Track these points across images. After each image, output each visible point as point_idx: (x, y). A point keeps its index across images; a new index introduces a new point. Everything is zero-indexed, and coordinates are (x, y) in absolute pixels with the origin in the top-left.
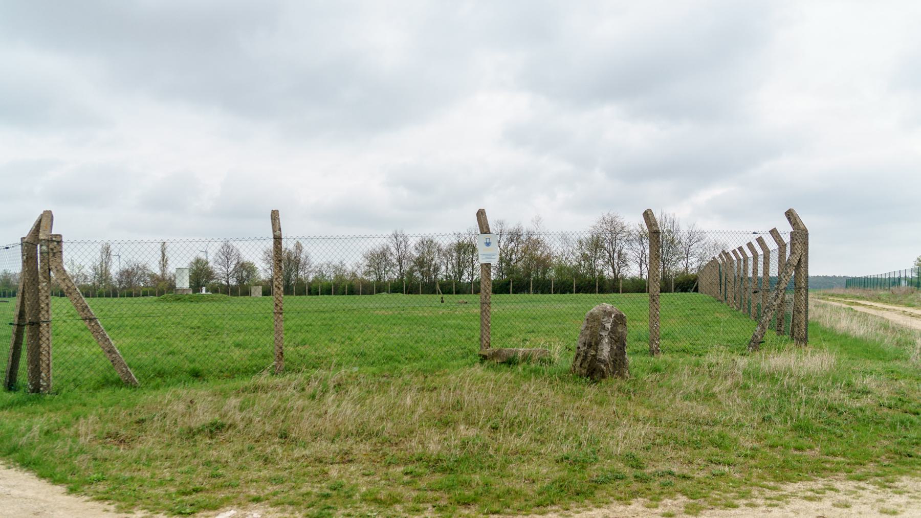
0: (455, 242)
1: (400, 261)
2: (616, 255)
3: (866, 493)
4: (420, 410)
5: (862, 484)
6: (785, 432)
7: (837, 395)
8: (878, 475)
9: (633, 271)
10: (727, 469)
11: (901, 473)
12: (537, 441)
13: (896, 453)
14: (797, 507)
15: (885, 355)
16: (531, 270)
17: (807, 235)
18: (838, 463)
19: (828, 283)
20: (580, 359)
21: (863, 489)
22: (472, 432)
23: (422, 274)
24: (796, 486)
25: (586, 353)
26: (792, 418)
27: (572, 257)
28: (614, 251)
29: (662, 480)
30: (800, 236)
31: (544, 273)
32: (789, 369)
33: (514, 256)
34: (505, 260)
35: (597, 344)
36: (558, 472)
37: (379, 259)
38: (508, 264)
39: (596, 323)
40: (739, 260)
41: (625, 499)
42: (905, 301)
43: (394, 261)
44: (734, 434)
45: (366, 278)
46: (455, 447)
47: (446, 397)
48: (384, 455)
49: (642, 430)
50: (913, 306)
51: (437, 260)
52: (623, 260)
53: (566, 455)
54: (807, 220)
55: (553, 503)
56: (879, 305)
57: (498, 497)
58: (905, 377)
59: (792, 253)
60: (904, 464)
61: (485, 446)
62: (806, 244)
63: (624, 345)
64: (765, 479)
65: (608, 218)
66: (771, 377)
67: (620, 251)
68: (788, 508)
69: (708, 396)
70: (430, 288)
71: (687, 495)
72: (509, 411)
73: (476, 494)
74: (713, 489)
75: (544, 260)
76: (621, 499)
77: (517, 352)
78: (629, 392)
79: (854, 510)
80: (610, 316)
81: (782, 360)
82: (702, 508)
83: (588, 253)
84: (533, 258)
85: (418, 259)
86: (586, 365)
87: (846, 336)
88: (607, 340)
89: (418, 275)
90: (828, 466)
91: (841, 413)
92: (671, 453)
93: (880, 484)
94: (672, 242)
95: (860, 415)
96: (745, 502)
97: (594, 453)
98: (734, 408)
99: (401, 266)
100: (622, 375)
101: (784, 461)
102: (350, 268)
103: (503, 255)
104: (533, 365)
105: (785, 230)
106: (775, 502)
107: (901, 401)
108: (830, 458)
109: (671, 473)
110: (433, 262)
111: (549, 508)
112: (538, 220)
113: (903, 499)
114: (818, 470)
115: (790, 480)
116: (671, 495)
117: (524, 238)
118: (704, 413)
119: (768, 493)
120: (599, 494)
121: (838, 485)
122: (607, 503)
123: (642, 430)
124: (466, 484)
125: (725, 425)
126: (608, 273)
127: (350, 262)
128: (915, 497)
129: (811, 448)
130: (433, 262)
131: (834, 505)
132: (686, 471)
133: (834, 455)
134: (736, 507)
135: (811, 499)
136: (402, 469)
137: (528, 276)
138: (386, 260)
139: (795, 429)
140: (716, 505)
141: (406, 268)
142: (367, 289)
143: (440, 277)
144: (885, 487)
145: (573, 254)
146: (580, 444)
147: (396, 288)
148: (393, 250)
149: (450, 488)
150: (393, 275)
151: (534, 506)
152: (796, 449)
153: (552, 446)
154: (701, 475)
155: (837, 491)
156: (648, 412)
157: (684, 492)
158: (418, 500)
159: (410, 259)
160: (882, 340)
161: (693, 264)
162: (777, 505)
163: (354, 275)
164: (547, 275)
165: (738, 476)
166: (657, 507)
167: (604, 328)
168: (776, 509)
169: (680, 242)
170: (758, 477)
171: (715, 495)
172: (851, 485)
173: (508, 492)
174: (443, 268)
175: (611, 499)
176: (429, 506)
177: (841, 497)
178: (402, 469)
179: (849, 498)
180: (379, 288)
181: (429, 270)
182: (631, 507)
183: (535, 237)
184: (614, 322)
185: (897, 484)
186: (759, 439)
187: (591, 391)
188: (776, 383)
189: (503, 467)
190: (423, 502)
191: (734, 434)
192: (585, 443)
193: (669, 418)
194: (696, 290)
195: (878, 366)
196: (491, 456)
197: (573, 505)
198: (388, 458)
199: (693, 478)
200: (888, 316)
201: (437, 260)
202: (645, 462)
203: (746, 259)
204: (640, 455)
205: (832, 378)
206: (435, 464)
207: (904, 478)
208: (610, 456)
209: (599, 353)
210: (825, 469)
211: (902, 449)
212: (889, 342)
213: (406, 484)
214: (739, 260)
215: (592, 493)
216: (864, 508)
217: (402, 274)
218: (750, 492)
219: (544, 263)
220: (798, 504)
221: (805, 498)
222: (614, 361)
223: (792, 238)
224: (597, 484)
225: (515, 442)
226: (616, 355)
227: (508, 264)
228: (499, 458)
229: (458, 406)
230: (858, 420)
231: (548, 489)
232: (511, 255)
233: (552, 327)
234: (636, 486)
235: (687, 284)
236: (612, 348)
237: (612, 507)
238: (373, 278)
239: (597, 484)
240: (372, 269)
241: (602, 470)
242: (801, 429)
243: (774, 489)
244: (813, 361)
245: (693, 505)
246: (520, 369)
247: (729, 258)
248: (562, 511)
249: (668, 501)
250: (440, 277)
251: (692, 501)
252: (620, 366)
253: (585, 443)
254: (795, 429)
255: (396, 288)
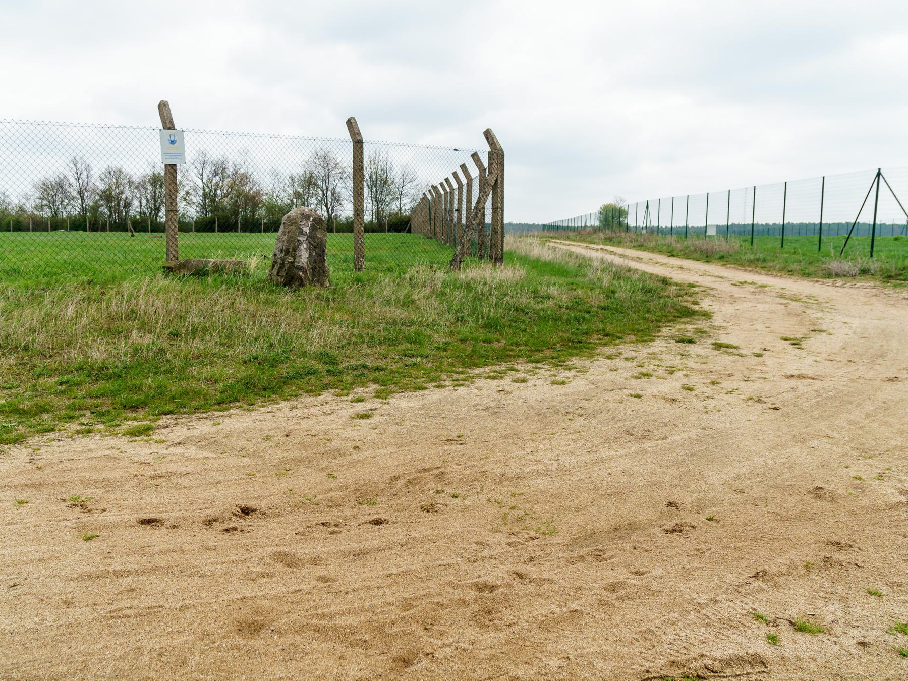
0: (151, 173)
1: (81, 193)
2: (329, 193)
3: (542, 372)
4: (85, 321)
5: (539, 365)
6: (477, 329)
7: (524, 300)
8: (553, 358)
9: (346, 211)
10: (419, 359)
11: (572, 355)
12: (223, 345)
13: (569, 341)
14: (481, 385)
15: (568, 273)
16: (238, 207)
17: (503, 156)
18: (520, 351)
19: (525, 229)
20: (276, 267)
21: (540, 368)
22: (147, 340)
23: (110, 211)
24: (482, 370)
25: (283, 260)
26: (483, 318)
27: (283, 194)
28: (327, 189)
29: (355, 373)
30: (497, 155)
31: (253, 212)
32: (485, 279)
33: (219, 192)
34: (209, 197)
35: (295, 250)
36: (243, 372)
37: (53, 190)
38: (213, 201)
39: (294, 228)
40: (446, 192)
41: (315, 391)
42: (589, 239)
43: (75, 194)
44: (429, 332)
45: (36, 213)
46: (126, 354)
47: (118, 306)
48: (34, 367)
49: (337, 331)
50: (594, 243)
51: (127, 194)
52: (337, 199)
53: (254, 354)
54: (503, 142)
55: (236, 400)
56: (567, 242)
57: (173, 398)
58: (582, 288)
59: (490, 173)
60: (576, 348)
61: (162, 351)
62: (502, 165)
63: (324, 251)
64: (454, 366)
65: (321, 153)
66: (468, 286)
67: (334, 189)
68: (472, 387)
69: (408, 303)
70: (120, 226)
71: (378, 383)
72: (194, 318)
73: (147, 397)
74: (404, 377)
75: (254, 197)
76: (311, 391)
77: (207, 263)
78: (327, 299)
79: (530, 384)
80: (309, 219)
81: (480, 272)
82: (392, 393)
83: (301, 190)
84: (240, 194)
85: (104, 192)
86: (283, 273)
87: (538, 261)
88: (305, 246)
89: (104, 210)
90: (512, 353)
91: (527, 313)
92: (365, 349)
93: (553, 364)
94: (386, 182)
95: (542, 313)
96: (433, 384)
97: (285, 352)
98: (431, 310)
99: (83, 199)
100: (322, 285)
101: (473, 351)
102: (16, 201)
103: (207, 190)
104: (225, 277)
105: (484, 150)
106: (461, 382)
107: (576, 304)
108: (514, 347)
109: (364, 366)
110: (124, 196)
111: (232, 405)
112: (245, 152)
113: (571, 374)
114: (503, 356)
115: (476, 366)
116: (363, 385)
117: (230, 171)
118: (402, 316)
119: (456, 376)
120: (288, 390)
121: (519, 367)
122: (296, 396)
123: (337, 331)
124: (138, 389)
125: (421, 325)
126: (323, 213)
127: (15, 194)
128: (581, 371)
129: (498, 341)
130: (124, 196)
131: (514, 381)
132: (380, 363)
133: (517, 344)
134: (426, 388)
135: (494, 378)
136: (56, 379)
137: (234, 212)
138: (64, 192)
139: (485, 326)
140: (406, 389)
141: (89, 202)
142: (39, 226)
143: (132, 213)
144: (557, 366)
145: (284, 191)
146: (271, 345)
147: (77, 225)
148: (72, 180)
149: (113, 394)
150: (74, 209)
151: (215, 404)
152: (484, 341)
153: (239, 349)
154: (394, 367)
155: (517, 371)
156: (345, 317)
157: (375, 381)
158: (74, 408)
159: (94, 191)
160: (567, 263)
161: (406, 205)
162: (463, 385)
163: (21, 209)
164: (256, 214)
165: (429, 365)
166: (347, 395)
167: (302, 232)
168: (462, 388)
169: (393, 182)
170: (448, 365)
171: (405, 381)
172: (529, 366)
173: (186, 393)
174: (136, 203)
175: (301, 392)
176: (88, 413)
177: (520, 375)
178: (56, 379)
179: (527, 376)
180: (56, 225)
181: (118, 205)
182: (321, 398)
183: (242, 171)
184: (313, 226)
185: (567, 363)
186: (451, 334)
187: (286, 298)
188: (471, 291)
189: (183, 369)
190: (80, 409)
191: (429, 332)
192: (277, 343)
193: (367, 321)
194: (409, 231)
195: (562, 280)
196: (168, 361)
197: (259, 401)
198: (37, 371)
199: (386, 369)
200: (573, 249)
201: (127, 194)
202: (340, 359)
203: (452, 190)
204: (335, 353)
205: (520, 285)
206: (100, 372)
207: (573, 359)
208: (304, 355)
209: (297, 259)
210: (509, 356)
211: (574, 337)
212: (572, 264)
213: (57, 394)
214: (446, 192)
215: (281, 387)
216: (538, 382)
217: (84, 209)
218: (439, 376)
219: (252, 200)
220: (481, 383)
221: (489, 377)
222: (314, 269)
223: (490, 158)
224: (286, 380)
225: (196, 345)
226: (315, 262)
227: (213, 201)
228: (177, 363)
229: (132, 315)
230: (540, 317)
231: (232, 387)
232: (216, 191)
233: (256, 253)
234: (327, 379)
235: (400, 225)
236: (310, 255)
237: (302, 399)
238: (47, 214)
239: (286, 380)
240: (45, 202)
241: (294, 367)
242: (491, 325)
243: (462, 373)
244: (506, 274)
245: (383, 391)
246: (210, 280)
247: (437, 192)
248: (246, 406)
249: (360, 390)
250: (132, 213)
251: (383, 388)
252: (320, 274)
253: (277, 343)
254: (485, 326)
255: (77, 225)
